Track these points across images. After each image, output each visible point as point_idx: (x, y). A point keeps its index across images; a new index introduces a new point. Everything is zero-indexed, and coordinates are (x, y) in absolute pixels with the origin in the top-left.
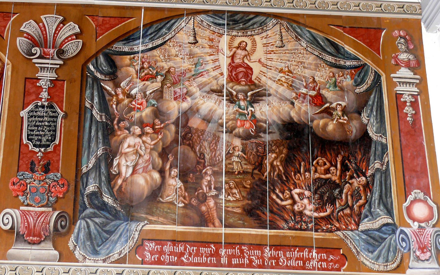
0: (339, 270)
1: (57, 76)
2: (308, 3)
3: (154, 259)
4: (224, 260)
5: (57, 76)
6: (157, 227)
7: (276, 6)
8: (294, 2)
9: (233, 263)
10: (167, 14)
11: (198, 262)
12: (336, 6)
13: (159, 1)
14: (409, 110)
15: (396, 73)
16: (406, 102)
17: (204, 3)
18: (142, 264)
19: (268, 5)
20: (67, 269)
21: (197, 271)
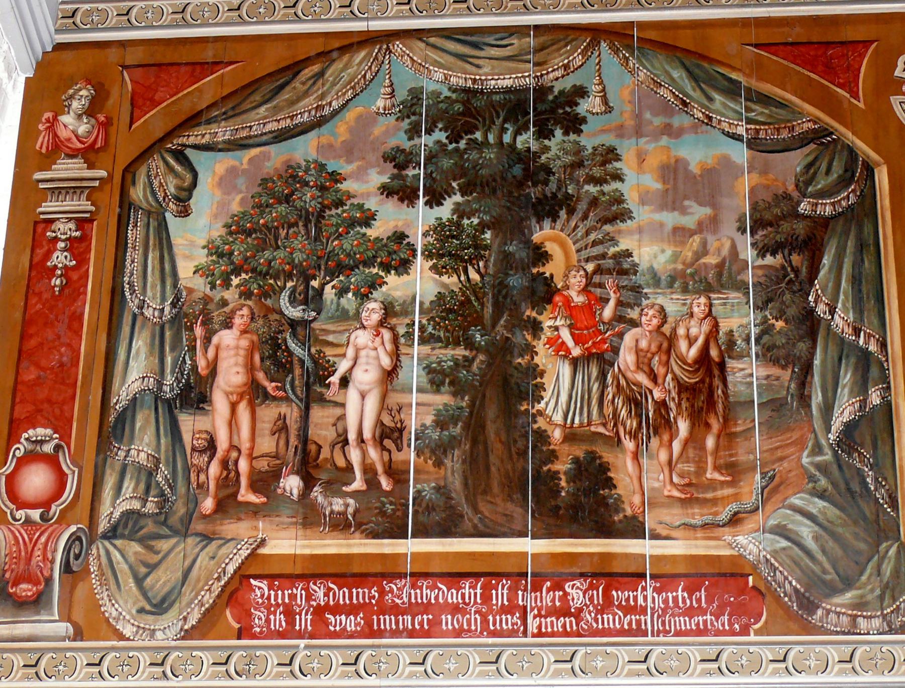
0: (745, 631)
1: (93, 208)
2: (223, 8)
3: (421, 624)
4: (304, 621)
5: (93, 208)
6: (598, 545)
7: (199, 21)
8: (300, 5)
9: (444, 627)
10: (319, 46)
11: (604, 628)
12: (407, 7)
13: (611, 5)
14: (60, 258)
15: (51, 170)
16: (56, 240)
17: (583, 7)
18: (239, 638)
19: (402, 11)
20: (712, 651)
21: (843, 647)
